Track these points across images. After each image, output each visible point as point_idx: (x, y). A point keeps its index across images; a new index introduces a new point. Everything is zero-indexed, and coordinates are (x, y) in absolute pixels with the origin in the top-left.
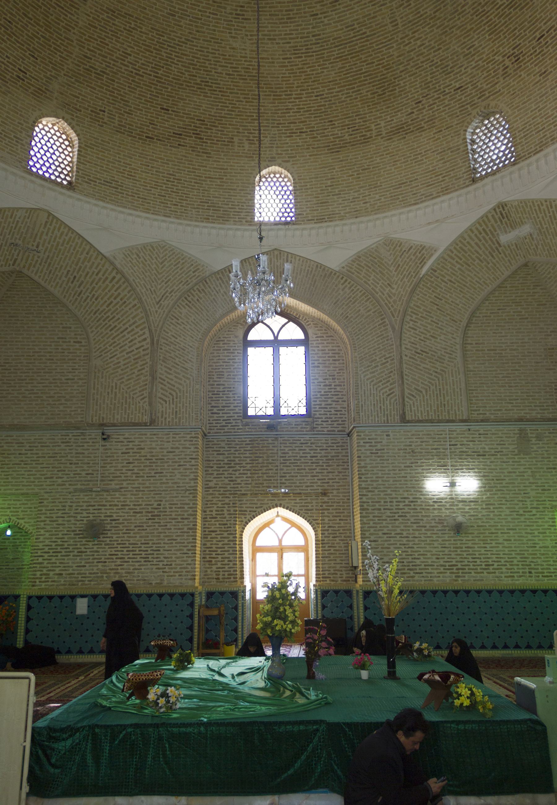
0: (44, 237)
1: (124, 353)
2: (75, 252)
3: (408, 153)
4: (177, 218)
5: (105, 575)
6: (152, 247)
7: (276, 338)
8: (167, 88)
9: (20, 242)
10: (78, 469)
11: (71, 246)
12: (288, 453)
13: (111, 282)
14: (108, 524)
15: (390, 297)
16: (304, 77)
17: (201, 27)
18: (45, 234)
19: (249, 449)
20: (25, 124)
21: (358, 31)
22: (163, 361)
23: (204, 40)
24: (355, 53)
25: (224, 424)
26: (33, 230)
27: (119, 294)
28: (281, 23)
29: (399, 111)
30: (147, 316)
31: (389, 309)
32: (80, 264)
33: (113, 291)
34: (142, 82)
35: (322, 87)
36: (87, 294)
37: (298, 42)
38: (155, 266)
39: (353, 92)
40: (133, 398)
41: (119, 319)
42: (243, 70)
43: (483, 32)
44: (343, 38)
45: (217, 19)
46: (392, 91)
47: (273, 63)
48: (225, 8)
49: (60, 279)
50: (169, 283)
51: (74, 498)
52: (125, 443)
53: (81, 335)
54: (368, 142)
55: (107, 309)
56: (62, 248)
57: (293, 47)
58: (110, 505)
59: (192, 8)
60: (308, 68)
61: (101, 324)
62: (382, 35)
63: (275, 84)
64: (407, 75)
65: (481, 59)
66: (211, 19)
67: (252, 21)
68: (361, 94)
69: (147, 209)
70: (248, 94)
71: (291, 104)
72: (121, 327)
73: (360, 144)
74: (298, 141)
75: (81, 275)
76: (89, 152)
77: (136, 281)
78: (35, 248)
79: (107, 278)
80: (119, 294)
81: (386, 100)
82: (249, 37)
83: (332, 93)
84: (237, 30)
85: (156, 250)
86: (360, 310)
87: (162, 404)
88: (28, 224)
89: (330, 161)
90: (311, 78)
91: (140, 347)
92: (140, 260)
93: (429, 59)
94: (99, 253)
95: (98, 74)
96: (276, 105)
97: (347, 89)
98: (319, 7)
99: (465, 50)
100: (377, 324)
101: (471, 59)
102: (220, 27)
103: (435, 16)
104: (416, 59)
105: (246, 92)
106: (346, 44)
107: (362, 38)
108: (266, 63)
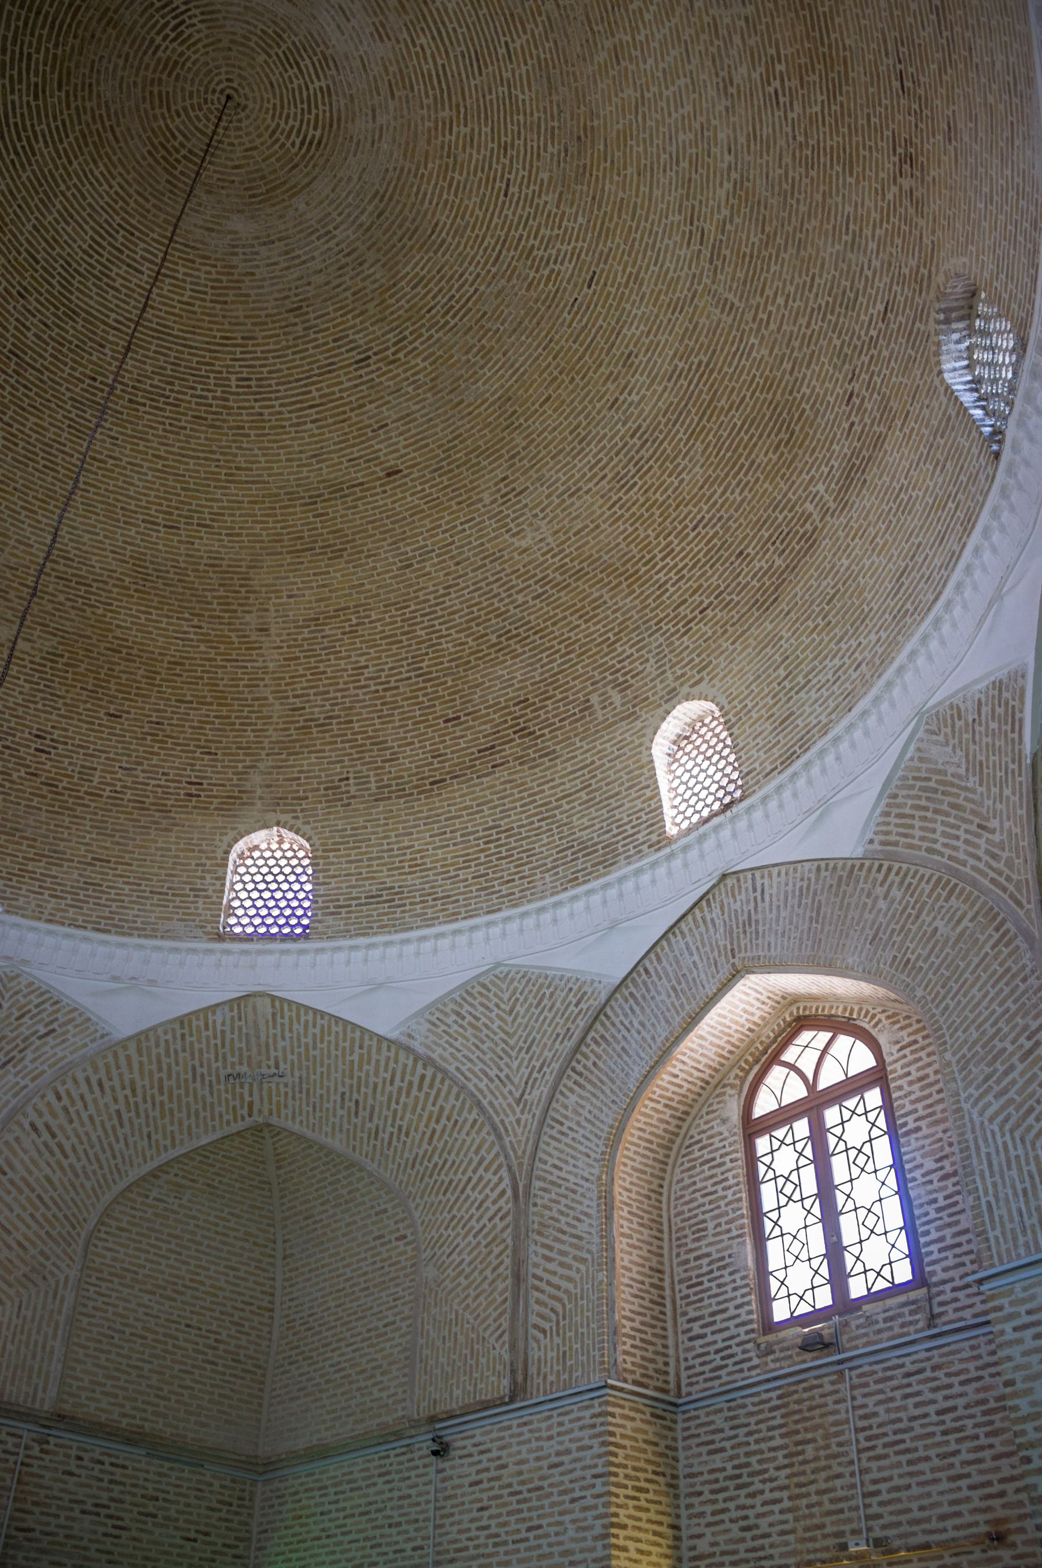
0: (281, 1044)
1: (470, 1238)
2: (339, 1053)
3: (883, 506)
4: (515, 906)
6: (484, 986)
7: (811, 1087)
8: (446, 682)
9: (244, 1069)
11: (329, 1042)
12: (875, 1414)
13: (420, 1089)
15: (995, 857)
16: (658, 513)
17: (460, 554)
18: (279, 1038)
19: (779, 1421)
20: (208, 862)
21: (689, 370)
22: (539, 1233)
23: (473, 571)
24: (708, 406)
25: (718, 1362)
26: (258, 1037)
27: (442, 1109)
28: (574, 458)
29: (831, 443)
31: (1005, 890)
32: (356, 1073)
33: (429, 1107)
34: (399, 698)
35: (695, 506)
37: (616, 465)
38: (498, 1022)
39: (745, 475)
41: (454, 1162)
42: (557, 574)
43: (841, 181)
44: (676, 400)
45: (476, 525)
46: (799, 419)
47: (597, 527)
48: (481, 500)
49: (335, 1116)
50: (534, 1048)
54: (815, 541)
55: (430, 1149)
56: (317, 1053)
57: (613, 478)
59: (432, 536)
60: (655, 493)
61: (428, 1184)
62: (725, 343)
63: (619, 559)
64: (804, 369)
65: (874, 226)
66: (468, 532)
67: (531, 488)
68: (759, 465)
69: (453, 914)
70: (584, 607)
71: (661, 575)
72: (460, 1180)
73: (804, 556)
74: (704, 629)
76: (331, 860)
77: (463, 1069)
78: (273, 1070)
80: (442, 1109)
81: (803, 442)
82: (541, 516)
83: (716, 502)
84: (517, 518)
85: (494, 989)
86: (936, 929)
87: (537, 1341)
88: (244, 1031)
89: (770, 627)
90: (670, 505)
91: (495, 1215)
92: (465, 1023)
93: (813, 309)
94: (381, 1039)
95: (323, 725)
96: (638, 591)
97: (734, 478)
98: (612, 387)
99: (844, 237)
100: (987, 948)
101: (863, 242)
102: (488, 533)
103: (768, 236)
104: (796, 330)
105: (579, 605)
106: (686, 405)
107: (702, 376)
108: (587, 535)
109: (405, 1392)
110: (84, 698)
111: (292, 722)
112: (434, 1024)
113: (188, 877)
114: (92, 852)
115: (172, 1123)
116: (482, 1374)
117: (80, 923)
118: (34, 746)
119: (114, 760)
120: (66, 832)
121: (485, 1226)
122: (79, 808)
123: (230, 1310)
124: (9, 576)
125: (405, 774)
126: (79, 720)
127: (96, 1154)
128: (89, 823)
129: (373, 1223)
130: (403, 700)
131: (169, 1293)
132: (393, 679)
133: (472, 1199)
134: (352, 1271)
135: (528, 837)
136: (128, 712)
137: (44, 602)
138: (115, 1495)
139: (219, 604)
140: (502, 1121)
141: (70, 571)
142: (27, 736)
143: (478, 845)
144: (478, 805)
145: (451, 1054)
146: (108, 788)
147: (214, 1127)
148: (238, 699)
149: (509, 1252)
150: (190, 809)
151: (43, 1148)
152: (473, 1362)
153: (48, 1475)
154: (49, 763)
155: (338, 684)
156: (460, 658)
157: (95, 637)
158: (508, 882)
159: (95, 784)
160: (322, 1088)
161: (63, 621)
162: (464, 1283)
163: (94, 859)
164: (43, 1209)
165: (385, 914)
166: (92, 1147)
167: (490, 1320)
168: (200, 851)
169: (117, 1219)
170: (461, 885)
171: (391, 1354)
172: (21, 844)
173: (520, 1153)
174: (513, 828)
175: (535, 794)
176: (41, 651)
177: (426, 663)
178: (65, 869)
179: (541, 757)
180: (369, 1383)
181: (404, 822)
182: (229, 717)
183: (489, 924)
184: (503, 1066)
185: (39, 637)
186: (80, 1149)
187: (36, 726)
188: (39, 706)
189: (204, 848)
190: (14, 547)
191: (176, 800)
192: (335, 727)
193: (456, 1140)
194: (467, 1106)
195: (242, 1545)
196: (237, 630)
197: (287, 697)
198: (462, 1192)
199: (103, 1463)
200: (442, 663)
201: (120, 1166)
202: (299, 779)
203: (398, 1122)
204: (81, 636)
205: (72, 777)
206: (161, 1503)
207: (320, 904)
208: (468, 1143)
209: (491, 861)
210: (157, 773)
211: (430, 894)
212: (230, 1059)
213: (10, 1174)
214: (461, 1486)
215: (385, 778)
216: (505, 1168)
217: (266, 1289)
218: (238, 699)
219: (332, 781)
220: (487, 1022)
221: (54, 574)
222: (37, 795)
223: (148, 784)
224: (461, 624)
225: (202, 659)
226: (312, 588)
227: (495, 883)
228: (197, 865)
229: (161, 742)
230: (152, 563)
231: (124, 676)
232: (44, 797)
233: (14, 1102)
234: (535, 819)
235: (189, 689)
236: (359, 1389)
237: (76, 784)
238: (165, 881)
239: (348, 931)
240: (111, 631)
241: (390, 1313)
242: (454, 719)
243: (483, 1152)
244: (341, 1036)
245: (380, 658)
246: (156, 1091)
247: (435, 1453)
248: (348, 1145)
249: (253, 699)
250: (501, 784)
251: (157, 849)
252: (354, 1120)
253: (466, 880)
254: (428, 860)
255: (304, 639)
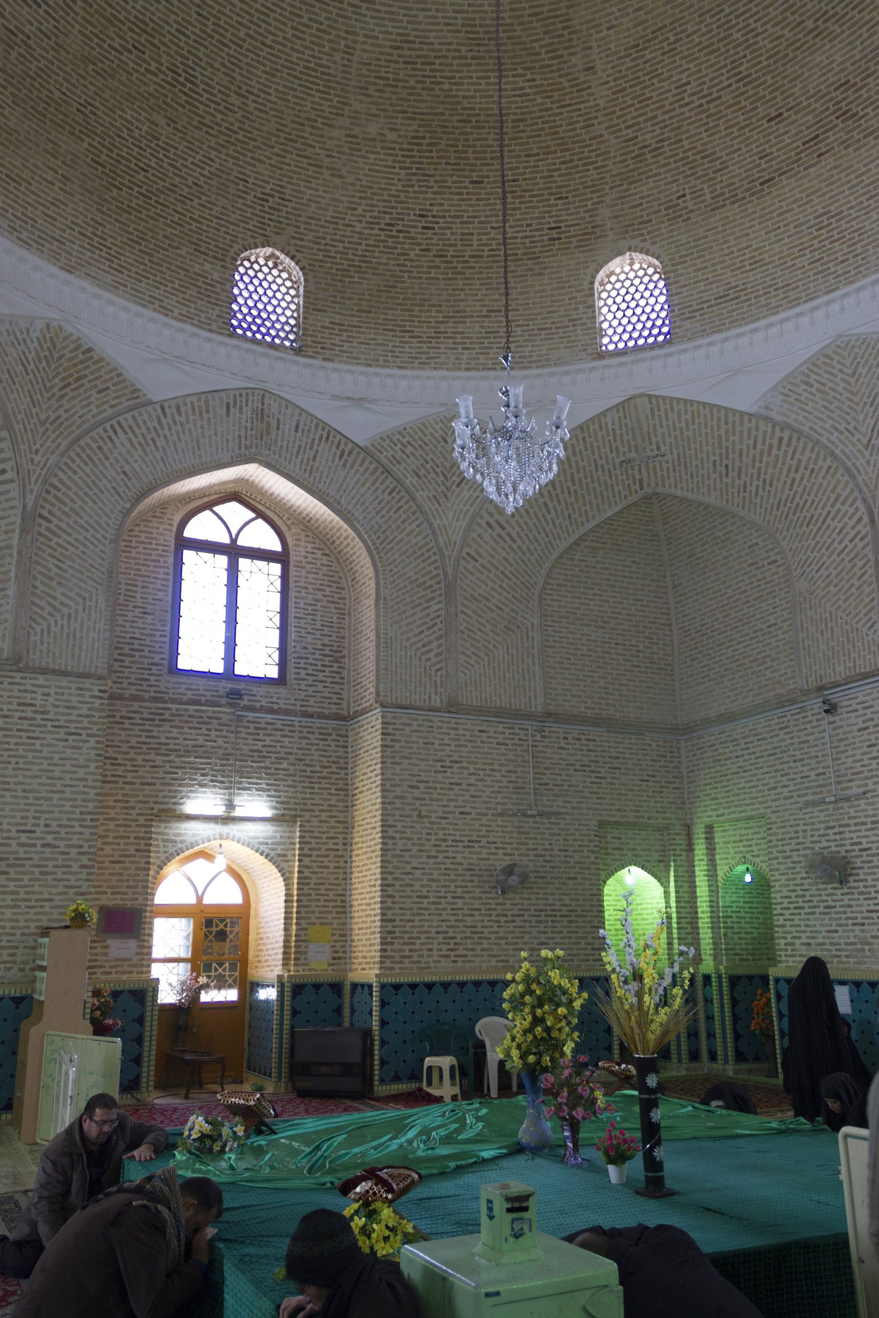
0: (660, 431)
1: (835, 556)
2: (709, 430)
4: (851, 283)
5: (867, 947)
9: (633, 455)
10: (805, 769)
11: (699, 424)
13: (779, 448)
14: (857, 857)
18: (658, 427)
20: (579, 295)
27: (799, 461)
30: (853, 477)
32: (724, 444)
36: (755, 483)
38: (843, 385)
40: (857, 629)
41: (813, 501)
49: (709, 479)
51: (807, 816)
52: (861, 712)
53: (773, 549)
55: (792, 493)
56: (690, 433)
58: (856, 824)
61: (792, 520)
69: (795, 300)
75: (733, 459)
77: (816, 427)
78: (656, 452)
79: (771, 446)
80: (799, 461)
85: (836, 358)
91: (855, 536)
92: (813, 390)
94: (742, 414)
95: (656, 149)
109: (793, 671)
110: (450, 172)
111: (628, 153)
112: (786, 395)
113: (565, 310)
114: (486, 306)
115: (585, 505)
116: (859, 654)
117: (490, 366)
118: (420, 225)
119: (485, 222)
120: (462, 293)
121: (846, 546)
122: (467, 271)
123: (641, 629)
124: (366, 73)
125: (736, 180)
126: (450, 193)
127: (534, 536)
128: (478, 282)
129: (747, 554)
130: (726, 109)
131: (600, 623)
132: (715, 89)
133: (832, 527)
134: (733, 590)
135: (858, 217)
136: (488, 177)
137: (399, 90)
138: (592, 758)
139: (547, 52)
140: (854, 464)
141: (414, 53)
142: (412, 217)
143: (811, 233)
144: (807, 196)
145: (804, 417)
146: (486, 248)
147: (616, 502)
148: (578, 142)
149: (871, 563)
150: (555, 252)
151: (498, 539)
152: (850, 646)
153: (549, 751)
154: (436, 237)
155: (664, 106)
156: (778, 52)
157: (447, 112)
158: (842, 262)
159: (475, 247)
160: (696, 459)
161: (418, 105)
162: (834, 590)
163: (488, 311)
164: (506, 580)
165: (734, 311)
166: (531, 531)
167: (861, 615)
168: (570, 287)
169: (556, 579)
170: (799, 272)
171: (778, 646)
172: (431, 311)
173: (872, 487)
174: (842, 212)
175: (862, 174)
176: (406, 137)
177: (745, 66)
178: (468, 325)
179: (865, 137)
180: (762, 668)
181: (741, 225)
182: (573, 161)
183: (828, 303)
184: (850, 420)
185: (402, 124)
186: (522, 534)
187: (418, 207)
188: (416, 188)
189: (573, 283)
190: (364, 43)
191: (543, 246)
192: (667, 149)
193: (814, 483)
194: (822, 456)
195: (677, 781)
196: (566, 75)
197: (620, 130)
198: (823, 522)
199: (580, 740)
200: (760, 62)
201: (553, 541)
202: (641, 204)
203: (762, 476)
204: (435, 114)
205: (456, 245)
206: (621, 760)
207: (677, 312)
208: (825, 485)
209: (824, 246)
210: (522, 226)
211: (772, 286)
212: (621, 450)
213: (480, 561)
214: (851, 732)
215: (718, 187)
216: (859, 500)
217: (664, 611)
218: (578, 142)
219: (671, 201)
220: (833, 386)
221: (401, 60)
222: (432, 267)
223: (517, 238)
224: (776, 16)
225: (540, 111)
226: (628, 14)
227: (831, 265)
228: (570, 299)
229: (520, 197)
230: (482, 26)
231: (478, 143)
232: (438, 267)
233: (472, 509)
234: (863, 198)
235: (535, 142)
236: (753, 673)
237: (460, 251)
238: (547, 318)
239: (705, 331)
240: (458, 103)
241: (771, 617)
242: (777, 117)
243: (839, 490)
244: (709, 417)
245: (700, 71)
246: (570, 483)
247: (826, 711)
248: (722, 499)
249: (590, 139)
250: (828, 171)
251: (536, 292)
252: (725, 480)
253: (804, 267)
254: (766, 256)
255: (628, 69)
